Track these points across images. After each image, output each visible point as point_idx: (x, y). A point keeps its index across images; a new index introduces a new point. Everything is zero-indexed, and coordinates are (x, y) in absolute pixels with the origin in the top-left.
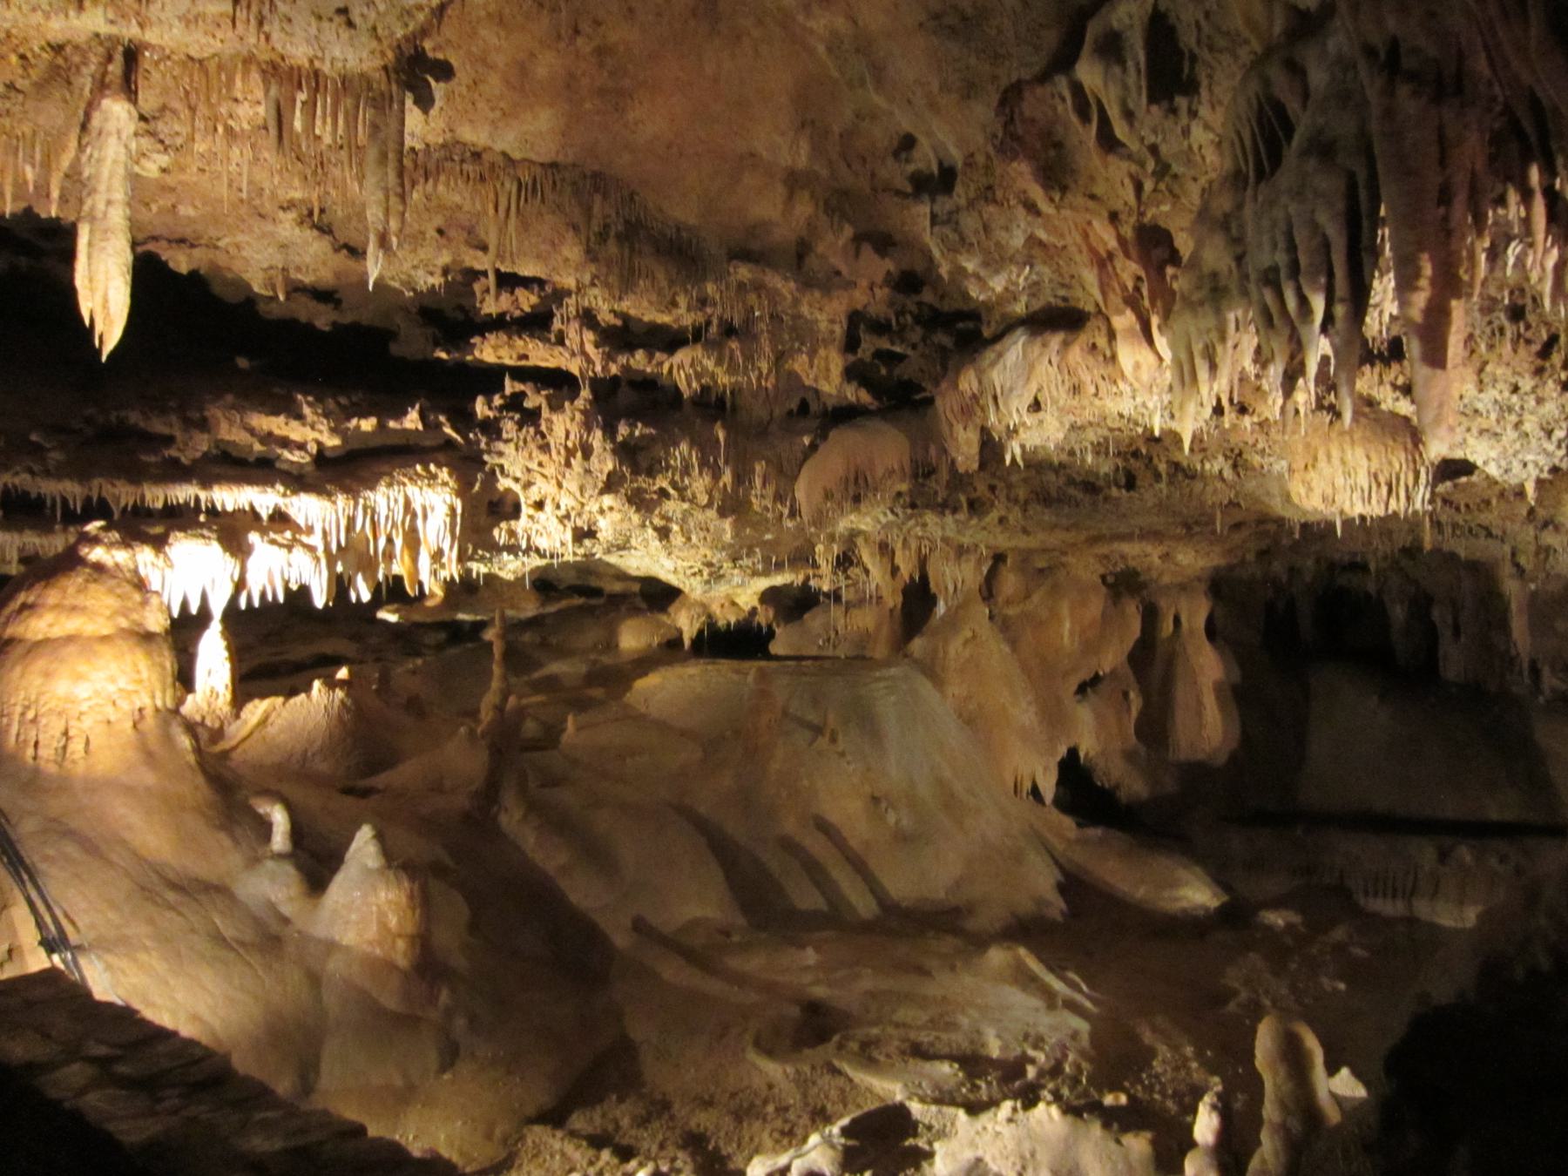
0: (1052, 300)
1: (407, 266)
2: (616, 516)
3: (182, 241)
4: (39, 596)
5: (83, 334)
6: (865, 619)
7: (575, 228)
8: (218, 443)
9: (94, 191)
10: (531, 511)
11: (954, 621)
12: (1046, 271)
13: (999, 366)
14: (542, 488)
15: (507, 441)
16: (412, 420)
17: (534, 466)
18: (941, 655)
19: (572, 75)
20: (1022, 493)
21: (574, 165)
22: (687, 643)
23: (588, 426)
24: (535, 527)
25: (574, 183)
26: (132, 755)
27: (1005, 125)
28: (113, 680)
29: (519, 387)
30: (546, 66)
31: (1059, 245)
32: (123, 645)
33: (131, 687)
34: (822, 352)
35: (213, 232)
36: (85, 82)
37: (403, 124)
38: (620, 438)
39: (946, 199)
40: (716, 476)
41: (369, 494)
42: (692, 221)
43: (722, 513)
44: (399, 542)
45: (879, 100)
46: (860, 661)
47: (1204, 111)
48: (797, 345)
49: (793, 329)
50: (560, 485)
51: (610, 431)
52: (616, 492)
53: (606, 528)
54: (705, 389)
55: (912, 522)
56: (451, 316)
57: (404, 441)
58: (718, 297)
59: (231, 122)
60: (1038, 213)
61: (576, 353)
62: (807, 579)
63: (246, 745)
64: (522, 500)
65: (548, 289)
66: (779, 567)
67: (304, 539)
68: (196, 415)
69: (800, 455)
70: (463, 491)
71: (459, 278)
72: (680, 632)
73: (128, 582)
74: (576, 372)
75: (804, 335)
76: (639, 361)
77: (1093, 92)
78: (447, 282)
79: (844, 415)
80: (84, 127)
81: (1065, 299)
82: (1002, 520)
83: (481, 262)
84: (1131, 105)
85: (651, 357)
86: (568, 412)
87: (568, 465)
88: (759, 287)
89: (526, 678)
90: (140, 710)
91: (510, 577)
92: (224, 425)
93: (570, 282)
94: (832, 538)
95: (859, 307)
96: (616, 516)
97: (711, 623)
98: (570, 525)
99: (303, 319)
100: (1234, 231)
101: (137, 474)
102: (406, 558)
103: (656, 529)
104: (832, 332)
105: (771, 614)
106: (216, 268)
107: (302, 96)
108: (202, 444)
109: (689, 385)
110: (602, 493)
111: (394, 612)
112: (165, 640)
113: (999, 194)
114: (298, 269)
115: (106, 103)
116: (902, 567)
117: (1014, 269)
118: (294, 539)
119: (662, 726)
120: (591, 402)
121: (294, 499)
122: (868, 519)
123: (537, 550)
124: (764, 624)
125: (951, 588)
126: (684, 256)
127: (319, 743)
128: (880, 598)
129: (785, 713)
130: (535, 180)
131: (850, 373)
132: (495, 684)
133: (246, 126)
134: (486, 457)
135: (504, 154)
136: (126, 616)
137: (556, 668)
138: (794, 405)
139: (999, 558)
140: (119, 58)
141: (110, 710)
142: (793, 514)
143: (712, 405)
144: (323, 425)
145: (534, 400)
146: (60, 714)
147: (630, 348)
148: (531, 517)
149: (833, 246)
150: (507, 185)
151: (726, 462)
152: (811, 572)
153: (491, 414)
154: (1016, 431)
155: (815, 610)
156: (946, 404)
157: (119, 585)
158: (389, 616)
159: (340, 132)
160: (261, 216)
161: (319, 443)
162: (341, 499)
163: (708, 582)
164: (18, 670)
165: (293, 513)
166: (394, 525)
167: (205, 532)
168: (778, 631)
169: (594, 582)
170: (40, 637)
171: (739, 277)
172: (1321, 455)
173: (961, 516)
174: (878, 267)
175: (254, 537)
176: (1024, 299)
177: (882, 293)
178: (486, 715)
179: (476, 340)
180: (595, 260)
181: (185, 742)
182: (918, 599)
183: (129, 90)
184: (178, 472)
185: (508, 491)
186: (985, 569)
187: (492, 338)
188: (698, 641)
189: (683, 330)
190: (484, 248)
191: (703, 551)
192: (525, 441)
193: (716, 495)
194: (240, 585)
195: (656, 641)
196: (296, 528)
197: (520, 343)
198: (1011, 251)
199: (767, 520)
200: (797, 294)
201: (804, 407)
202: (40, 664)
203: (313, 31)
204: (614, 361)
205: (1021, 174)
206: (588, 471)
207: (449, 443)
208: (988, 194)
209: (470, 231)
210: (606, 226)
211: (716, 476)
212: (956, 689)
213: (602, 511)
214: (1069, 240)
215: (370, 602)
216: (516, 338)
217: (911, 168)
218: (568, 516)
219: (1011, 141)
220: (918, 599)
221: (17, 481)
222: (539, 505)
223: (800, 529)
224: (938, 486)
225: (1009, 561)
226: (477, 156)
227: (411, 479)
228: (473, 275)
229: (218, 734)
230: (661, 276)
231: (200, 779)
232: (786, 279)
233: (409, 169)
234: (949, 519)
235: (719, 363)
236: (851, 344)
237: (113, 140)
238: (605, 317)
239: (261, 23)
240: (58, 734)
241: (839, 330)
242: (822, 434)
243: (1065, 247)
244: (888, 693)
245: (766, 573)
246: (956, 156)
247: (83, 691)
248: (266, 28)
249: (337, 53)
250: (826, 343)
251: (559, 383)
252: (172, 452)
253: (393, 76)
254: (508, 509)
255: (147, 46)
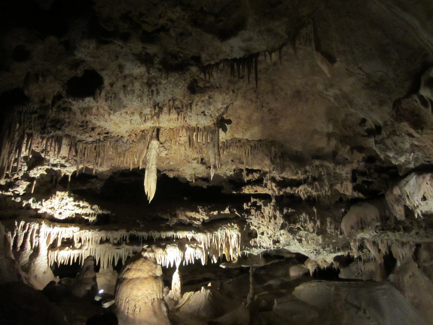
0: (424, 162)
1: (224, 170)
2: (285, 236)
3: (171, 170)
4: (131, 266)
5: (145, 197)
6: (371, 267)
7: (267, 156)
8: (179, 220)
9: (149, 162)
10: (260, 236)
11: (404, 269)
12: (420, 154)
13: (408, 186)
14: (263, 229)
15: (253, 215)
16: (227, 211)
17: (260, 222)
18: (401, 281)
19: (263, 117)
20: (423, 225)
21: (266, 140)
22: (311, 274)
23: (275, 210)
24: (262, 240)
25: (266, 144)
26: (151, 313)
27: (396, 112)
28: (147, 290)
29: (255, 200)
30: (256, 116)
31: (424, 145)
32: (151, 280)
33: (151, 292)
34: (345, 183)
35: (178, 167)
36: (148, 138)
37: (219, 137)
38: (284, 213)
39: (379, 136)
40: (315, 223)
41: (216, 232)
42: (300, 150)
43: (318, 234)
44: (224, 246)
45: (352, 110)
46: (370, 282)
48: (336, 181)
49: (334, 177)
50: (268, 228)
51: (281, 211)
52: (285, 229)
53: (282, 239)
54: (309, 197)
55: (383, 235)
56: (237, 182)
57: (225, 217)
58: (310, 170)
59: (179, 142)
60: (413, 137)
61: (270, 189)
62: (349, 253)
63: (183, 306)
64: (258, 232)
65: (262, 172)
66: (339, 250)
67: (199, 246)
68: (173, 213)
69: (341, 215)
70: (241, 230)
71: (238, 171)
72: (309, 270)
73: (153, 262)
74: (271, 194)
75: (338, 178)
76: (288, 190)
77: (427, 97)
78: (235, 173)
79: (354, 202)
80: (148, 148)
81: (428, 162)
82: (417, 233)
83: (243, 167)
85: (292, 188)
86: (269, 206)
87: (270, 221)
88: (322, 166)
89: (262, 285)
90: (154, 299)
91: (256, 254)
92: (180, 215)
93: (267, 170)
94: (355, 240)
95: (355, 168)
96: (285, 236)
97: (318, 267)
98: (272, 239)
99: (200, 185)
101: (160, 230)
102: (226, 250)
103: (297, 240)
104: (347, 177)
105: (338, 264)
106: (178, 175)
107: (195, 134)
108: (175, 221)
109: (304, 196)
110: (280, 229)
111: (224, 265)
112: (161, 278)
113: (398, 133)
114: (198, 174)
115: (152, 142)
116: (382, 249)
117: (408, 155)
118: (197, 246)
119: (304, 303)
120: (275, 203)
121: (197, 235)
122: (367, 234)
123: (263, 247)
124: (336, 268)
125: (401, 257)
126: (299, 160)
127: (203, 306)
128: (375, 259)
129: (346, 302)
130: (255, 145)
131: (355, 189)
132: (251, 291)
133: (183, 142)
134: (247, 220)
135: (247, 139)
136: (151, 272)
137: (272, 282)
138: (338, 199)
139: (418, 246)
140: (155, 131)
141: (146, 299)
142: (341, 233)
143: (311, 201)
144: (204, 214)
145: (259, 203)
146: (134, 300)
147: (286, 187)
148: (260, 237)
149: (344, 152)
150: (248, 147)
151: (318, 218)
152: (350, 251)
153: (248, 208)
154: (418, 206)
155: (353, 263)
156: (389, 198)
157: (150, 263)
158: (223, 266)
159: (204, 140)
160: (189, 162)
161: (203, 219)
162: (208, 234)
163: (316, 255)
164: (125, 288)
165: (196, 238)
166: (223, 241)
167: (175, 245)
168: (341, 270)
169: (281, 254)
170: (131, 278)
171: (316, 164)
173: (401, 232)
174: (360, 156)
175: (187, 246)
176: (413, 163)
177: (362, 164)
178: (249, 301)
179: (243, 188)
180: (273, 164)
181: (164, 309)
182: (389, 261)
183: (158, 138)
184: (169, 229)
185: (254, 229)
186: (413, 249)
187: (247, 187)
188: (315, 273)
189: (301, 180)
190: (243, 163)
191: (313, 246)
192: (257, 215)
193: (315, 228)
194: (183, 258)
195: (301, 274)
196: (197, 243)
197: (255, 187)
198: (405, 149)
199: (333, 236)
200: (334, 167)
201: (341, 200)
202: (130, 286)
203: (196, 118)
204: (281, 191)
205: (405, 126)
206: (276, 223)
207: (237, 216)
208: (394, 133)
209: (240, 159)
210: (276, 154)
211: (315, 223)
212: (410, 294)
213: (281, 235)
214: (427, 144)
215: (217, 263)
216: (253, 186)
217: (366, 128)
218: (271, 237)
219: (399, 115)
220: (389, 261)
221: (133, 232)
222: (263, 234)
223: (344, 238)
224: (391, 223)
225: (422, 246)
226: (240, 141)
227: (227, 228)
228: (242, 170)
229: (177, 303)
230: (292, 166)
231: (168, 321)
232: (330, 163)
233: (220, 147)
234: (397, 234)
235: (312, 189)
236: (354, 180)
237: (153, 150)
238: (278, 178)
239: (184, 119)
240: (133, 306)
241: (349, 176)
242: (348, 208)
243: (426, 146)
244: (383, 294)
245: (335, 252)
246: (381, 122)
247: (140, 293)
248: (185, 119)
249: (202, 122)
250: (346, 180)
251: (266, 198)
252: (168, 223)
253: (216, 125)
254: (254, 235)
255: (161, 127)
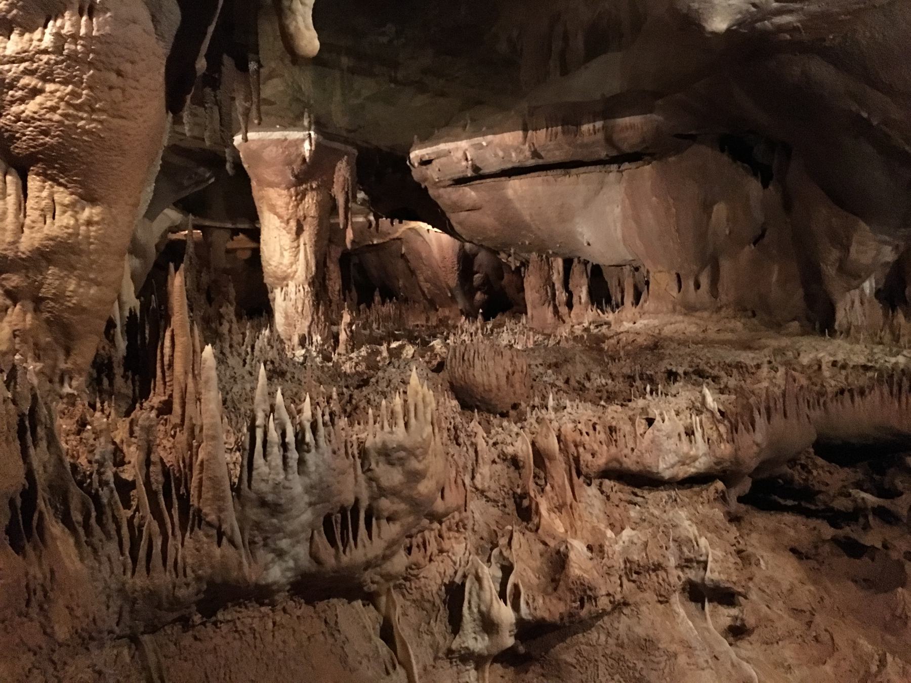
47: (450, 572)
84: (477, 584)
100: (374, 484)
172: (503, 381)
217: (734, 611)
